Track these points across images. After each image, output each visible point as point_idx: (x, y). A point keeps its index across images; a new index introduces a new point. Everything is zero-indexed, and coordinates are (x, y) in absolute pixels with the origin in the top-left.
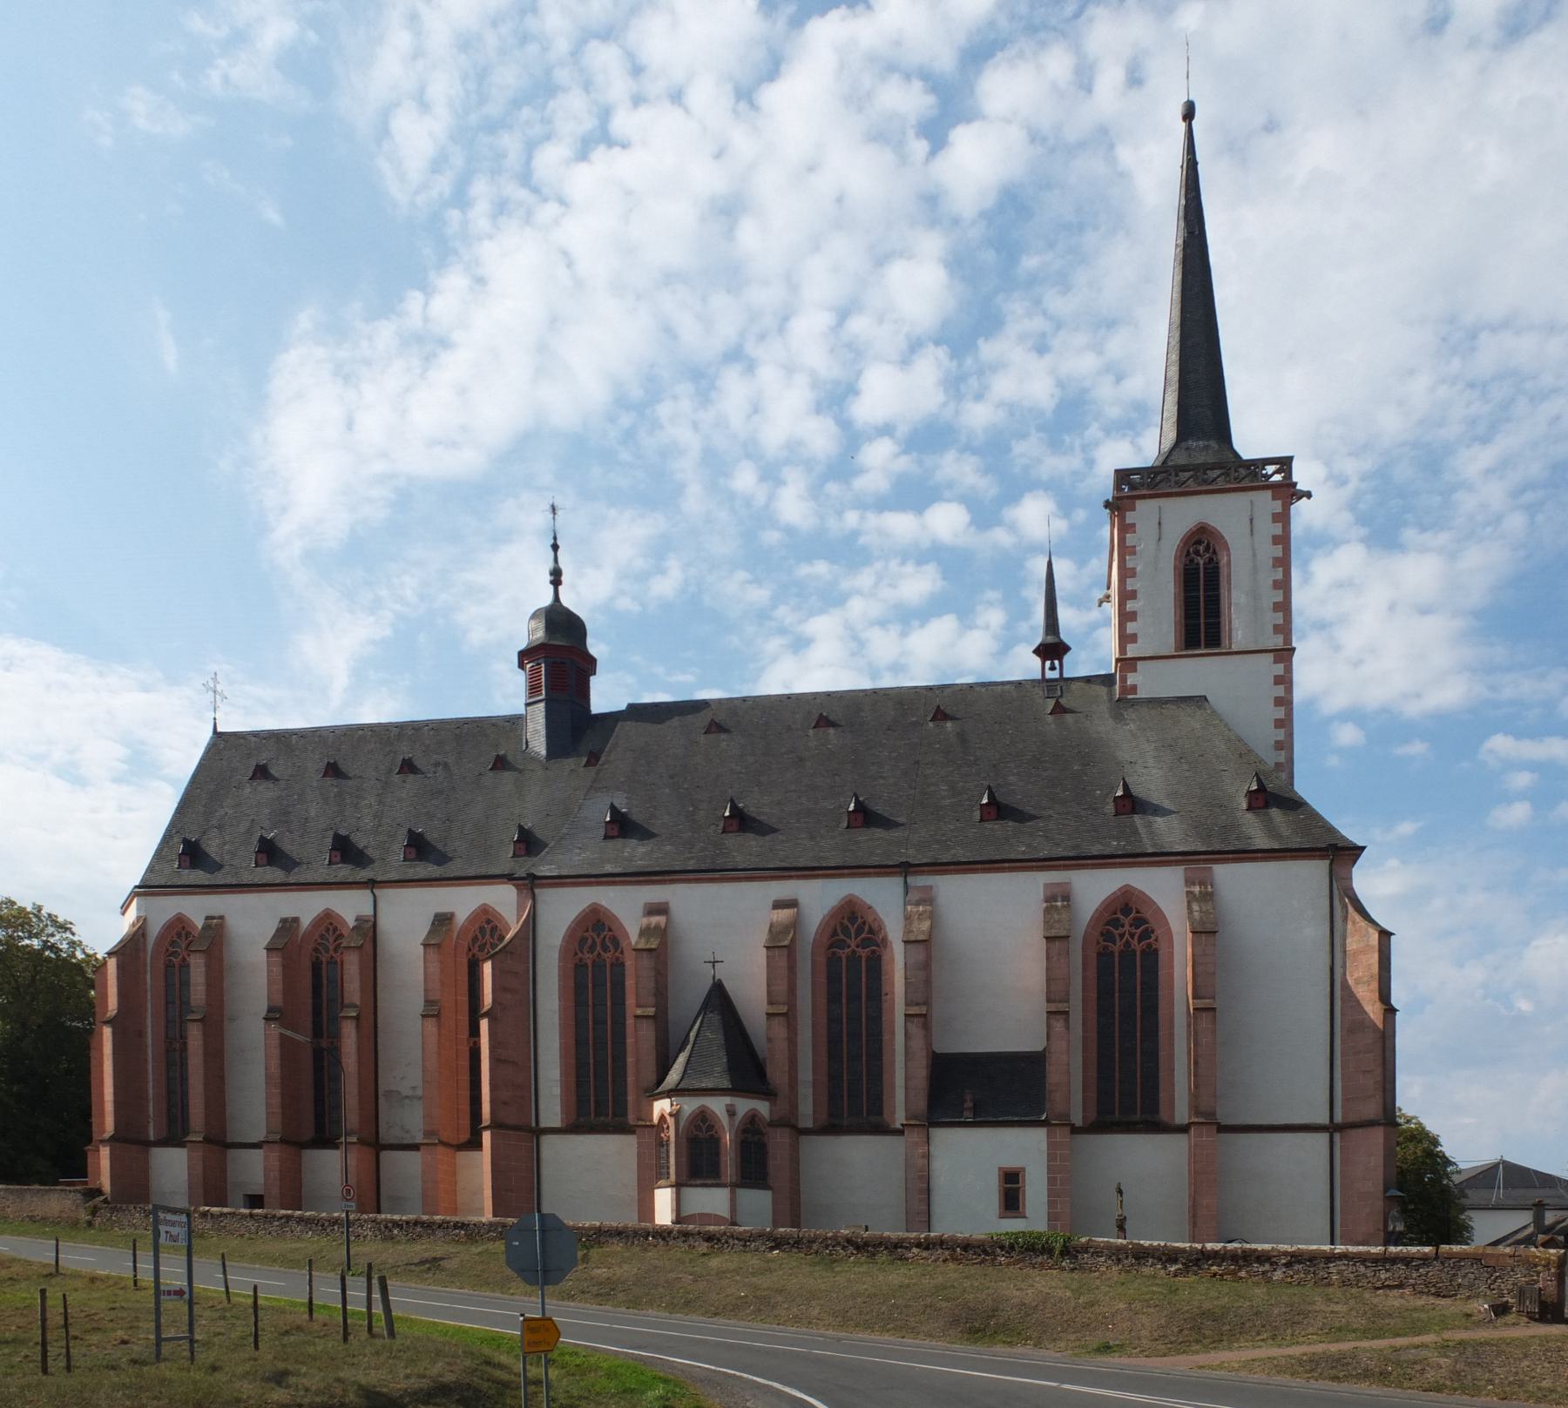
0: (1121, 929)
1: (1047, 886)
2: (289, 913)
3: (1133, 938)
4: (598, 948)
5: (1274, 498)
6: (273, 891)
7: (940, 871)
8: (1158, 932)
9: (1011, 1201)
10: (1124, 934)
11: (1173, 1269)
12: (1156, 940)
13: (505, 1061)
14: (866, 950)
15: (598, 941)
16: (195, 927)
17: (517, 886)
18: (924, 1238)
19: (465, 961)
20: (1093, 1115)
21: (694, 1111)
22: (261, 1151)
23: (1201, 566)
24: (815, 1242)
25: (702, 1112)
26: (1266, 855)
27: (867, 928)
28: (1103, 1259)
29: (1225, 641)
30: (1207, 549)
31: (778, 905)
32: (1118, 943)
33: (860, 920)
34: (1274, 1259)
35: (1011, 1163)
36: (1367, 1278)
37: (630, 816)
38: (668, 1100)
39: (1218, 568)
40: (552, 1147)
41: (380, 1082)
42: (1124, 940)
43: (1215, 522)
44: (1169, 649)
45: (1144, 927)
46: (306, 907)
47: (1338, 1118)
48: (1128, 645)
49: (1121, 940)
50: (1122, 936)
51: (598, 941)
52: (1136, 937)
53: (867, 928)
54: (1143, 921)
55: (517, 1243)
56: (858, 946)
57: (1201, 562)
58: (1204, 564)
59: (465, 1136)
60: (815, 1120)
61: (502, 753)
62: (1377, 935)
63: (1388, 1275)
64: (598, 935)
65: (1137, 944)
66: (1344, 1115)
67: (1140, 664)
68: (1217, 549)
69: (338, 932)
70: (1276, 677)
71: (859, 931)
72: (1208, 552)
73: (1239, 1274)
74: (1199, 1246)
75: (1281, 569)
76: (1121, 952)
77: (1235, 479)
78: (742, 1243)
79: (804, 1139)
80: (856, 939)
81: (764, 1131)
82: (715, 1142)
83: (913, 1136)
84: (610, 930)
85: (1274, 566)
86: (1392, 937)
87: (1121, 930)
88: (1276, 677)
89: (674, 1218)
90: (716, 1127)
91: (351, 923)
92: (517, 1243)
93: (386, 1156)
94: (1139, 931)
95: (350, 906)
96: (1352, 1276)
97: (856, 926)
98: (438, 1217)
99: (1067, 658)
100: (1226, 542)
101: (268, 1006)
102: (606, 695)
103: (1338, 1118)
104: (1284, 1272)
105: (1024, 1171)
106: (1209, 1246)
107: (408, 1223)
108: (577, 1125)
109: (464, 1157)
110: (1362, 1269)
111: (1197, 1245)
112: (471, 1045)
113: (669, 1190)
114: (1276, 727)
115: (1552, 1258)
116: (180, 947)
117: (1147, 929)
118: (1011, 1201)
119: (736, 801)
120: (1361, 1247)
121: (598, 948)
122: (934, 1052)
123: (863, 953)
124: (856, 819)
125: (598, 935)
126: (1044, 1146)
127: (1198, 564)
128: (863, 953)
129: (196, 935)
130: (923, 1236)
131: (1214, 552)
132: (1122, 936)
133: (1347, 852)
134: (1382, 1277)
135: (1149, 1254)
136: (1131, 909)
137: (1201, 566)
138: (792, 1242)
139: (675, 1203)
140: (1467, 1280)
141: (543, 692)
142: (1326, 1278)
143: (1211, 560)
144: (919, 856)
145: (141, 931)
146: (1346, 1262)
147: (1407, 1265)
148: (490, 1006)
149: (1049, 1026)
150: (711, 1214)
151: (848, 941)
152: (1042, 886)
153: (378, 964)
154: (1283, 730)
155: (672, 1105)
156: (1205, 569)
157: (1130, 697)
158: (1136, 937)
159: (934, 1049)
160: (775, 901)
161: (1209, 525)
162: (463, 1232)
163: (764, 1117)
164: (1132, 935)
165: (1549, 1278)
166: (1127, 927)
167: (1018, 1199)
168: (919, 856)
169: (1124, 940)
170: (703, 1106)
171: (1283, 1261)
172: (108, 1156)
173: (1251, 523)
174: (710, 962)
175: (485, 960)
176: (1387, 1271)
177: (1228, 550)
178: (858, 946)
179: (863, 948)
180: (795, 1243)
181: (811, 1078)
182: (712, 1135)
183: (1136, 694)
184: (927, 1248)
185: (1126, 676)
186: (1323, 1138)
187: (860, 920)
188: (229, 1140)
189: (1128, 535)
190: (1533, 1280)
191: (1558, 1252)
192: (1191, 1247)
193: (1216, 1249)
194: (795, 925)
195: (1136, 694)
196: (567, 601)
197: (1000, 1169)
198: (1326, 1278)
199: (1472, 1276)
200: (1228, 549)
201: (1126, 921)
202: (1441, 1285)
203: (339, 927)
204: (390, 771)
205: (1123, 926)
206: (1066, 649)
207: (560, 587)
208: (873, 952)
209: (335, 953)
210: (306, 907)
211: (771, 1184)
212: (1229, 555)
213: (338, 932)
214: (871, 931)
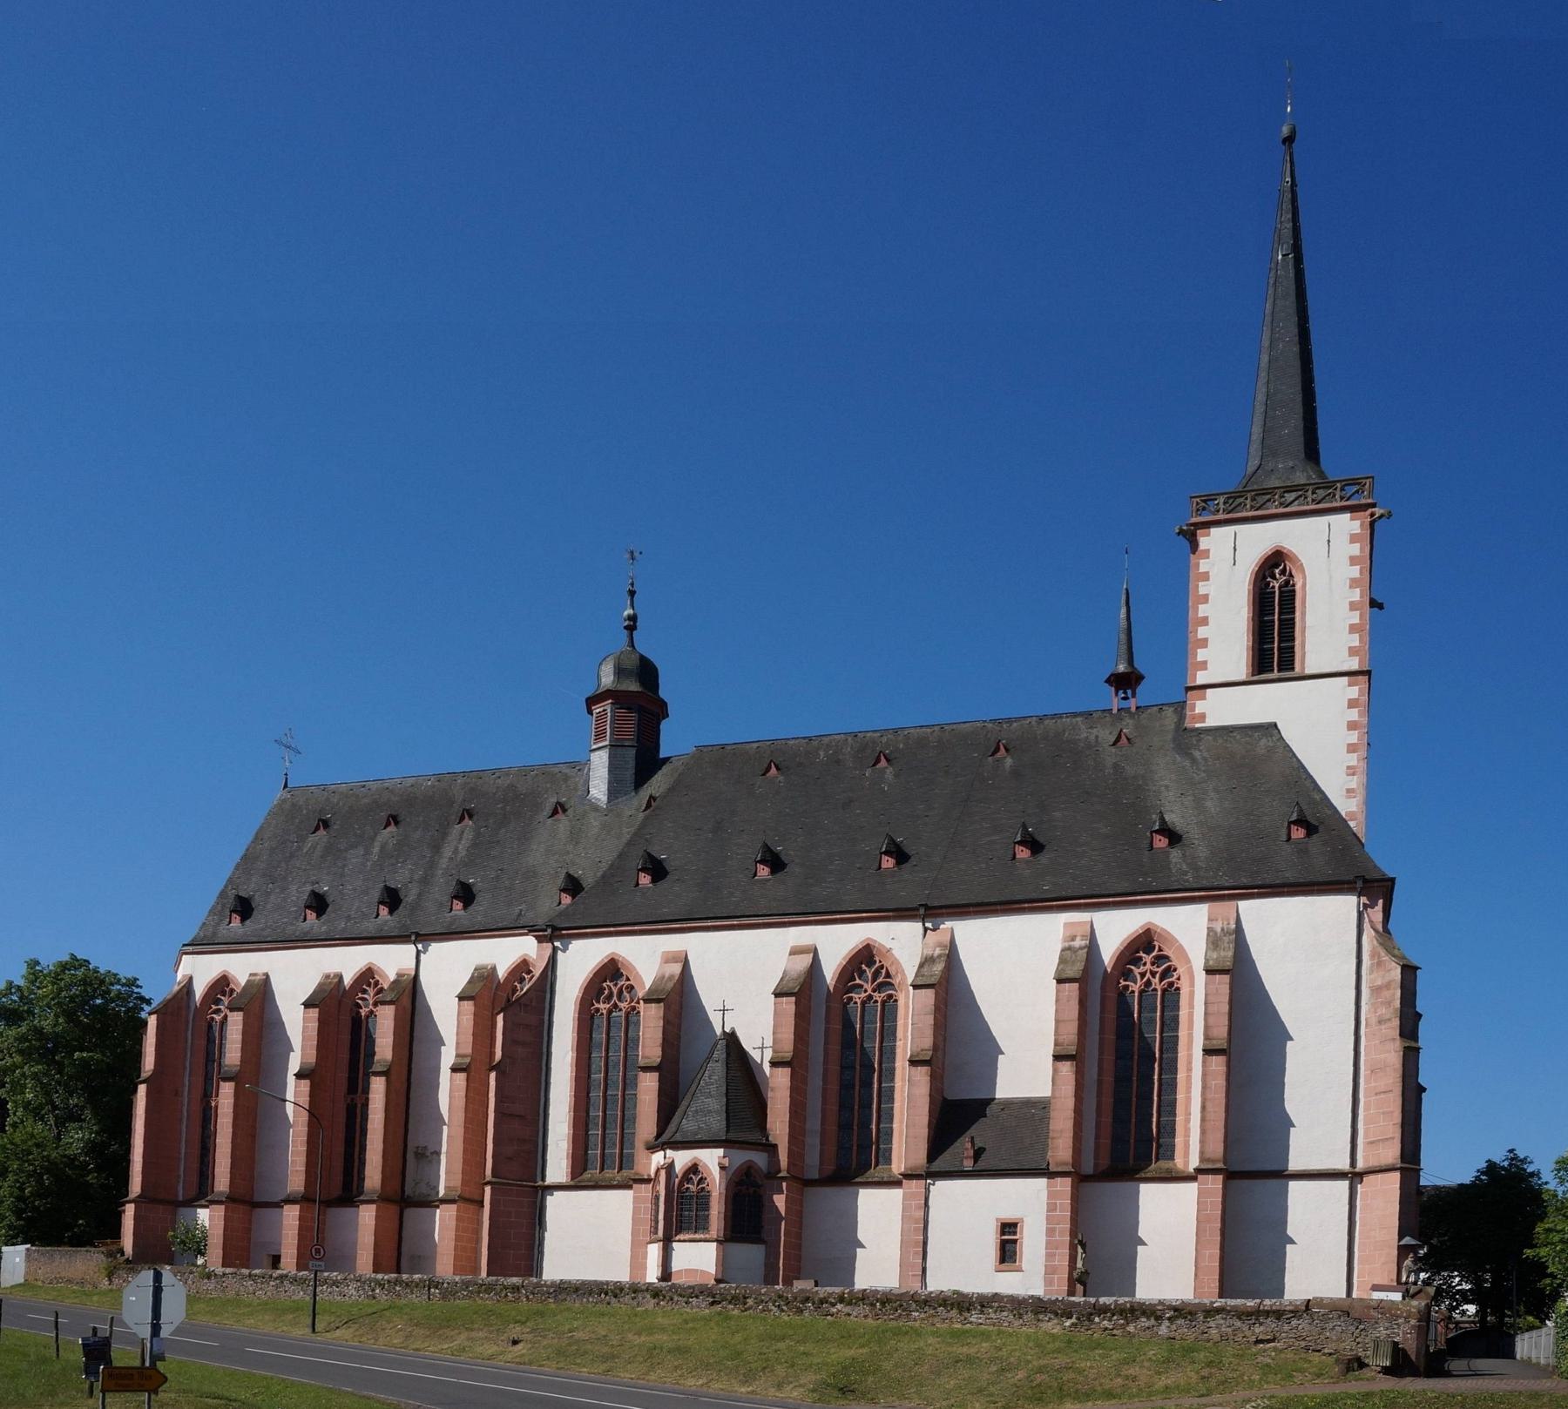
0: (1142, 967)
1: (1066, 925)
2: (333, 969)
3: (1154, 977)
4: (615, 998)
5: (1352, 519)
6: (480, 938)
7: (1304, 891)
8: (1181, 970)
9: (1008, 1252)
10: (1146, 972)
14: (882, 995)
15: (615, 991)
16: (237, 984)
18: (848, 1293)
20: (1105, 1163)
21: (687, 1163)
22: (208, 1210)
24: (750, 1297)
25: (749, 1168)
27: (884, 971)
28: (1005, 1314)
30: (1283, 572)
31: (795, 952)
33: (877, 964)
34: (1159, 1313)
35: (1009, 1215)
36: (1243, 1332)
38: (662, 1153)
39: (1294, 591)
42: (1145, 979)
43: (1290, 545)
45: (1165, 965)
46: (347, 962)
47: (1361, 1165)
48: (1198, 673)
49: (1142, 979)
50: (1143, 975)
51: (615, 991)
52: (1158, 976)
53: (884, 971)
54: (1162, 958)
55: (134, 1299)
56: (874, 991)
57: (1277, 585)
58: (1280, 587)
63: (1262, 1328)
65: (1158, 983)
67: (1209, 691)
68: (1294, 572)
69: (379, 986)
70: (1350, 701)
71: (876, 974)
72: (1285, 576)
73: (1128, 1329)
74: (1092, 1300)
75: (1358, 590)
76: (1141, 992)
77: (1313, 500)
78: (685, 1299)
79: (811, 1192)
80: (872, 984)
82: (703, 1199)
83: (915, 1186)
84: (628, 979)
85: (1351, 587)
86: (1418, 972)
87: (1142, 969)
88: (1350, 701)
89: (660, 1275)
90: (708, 1180)
92: (134, 1299)
93: (410, 1213)
94: (1160, 970)
95: (392, 960)
97: (873, 970)
98: (417, 1276)
100: (1302, 564)
101: (301, 1063)
102: (674, 739)
104: (1169, 1327)
105: (1023, 1221)
106: (1102, 1300)
107: (389, 1281)
108: (580, 1180)
109: (345, 1212)
111: (1091, 1299)
112: (349, 1101)
114: (1349, 752)
115: (1413, 1310)
116: (223, 1005)
117: (1170, 967)
118: (1008, 1252)
120: (1239, 1300)
121: (615, 998)
122: (945, 1099)
123: (878, 997)
124: (1160, 840)
125: (616, 985)
126: (1044, 1195)
128: (878, 997)
131: (1291, 575)
133: (1376, 884)
134: (1257, 1331)
135: (1047, 1308)
138: (730, 1298)
141: (608, 737)
142: (1206, 1333)
143: (1287, 583)
144: (1231, 881)
145: (185, 990)
146: (1225, 1316)
147: (1278, 1319)
148: (150, 1073)
149: (1055, 1071)
150: (697, 1270)
152: (1062, 925)
154: (1356, 754)
155: (665, 1157)
157: (1197, 725)
158: (1158, 976)
159: (946, 1096)
161: (1285, 548)
162: (437, 1291)
163: (761, 1170)
164: (1153, 974)
165: (1409, 1331)
166: (1148, 966)
168: (1231, 881)
169: (1145, 979)
171: (1167, 1315)
172: (133, 1217)
173: (1329, 544)
174: (720, 1010)
175: (498, 1013)
178: (874, 991)
179: (879, 993)
180: (733, 1299)
182: (704, 1188)
183: (1204, 722)
184: (850, 1304)
185: (1195, 704)
186: (1344, 1185)
187: (877, 964)
188: (257, 1199)
189: (1201, 561)
190: (1394, 1333)
191: (1420, 1303)
192: (1085, 1301)
195: (1204, 722)
196: (643, 648)
197: (997, 1219)
198: (1206, 1333)
199: (1339, 1329)
200: (1303, 571)
201: (1147, 958)
202: (1311, 1338)
203: (381, 981)
204: (637, 810)
205: (1145, 964)
207: (635, 632)
208: (890, 996)
209: (375, 1008)
210: (347, 962)
211: (766, 1239)
212: (1304, 578)
213: (379, 986)
214: (888, 975)
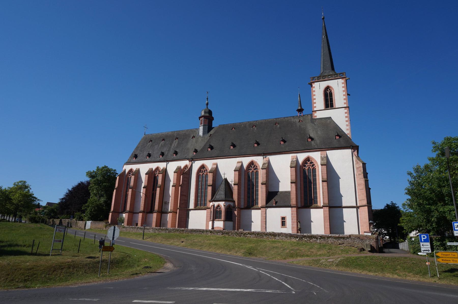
2: (151, 167)
8: (316, 165)
9: (283, 224)
11: (297, 239)
12: (315, 167)
13: (183, 195)
15: (203, 170)
16: (134, 170)
17: (189, 161)
19: (154, 177)
20: (303, 204)
23: (329, 93)
25: (230, 206)
26: (337, 148)
27: (256, 166)
29: (334, 107)
30: (330, 90)
31: (238, 162)
32: (307, 168)
35: (283, 216)
37: (213, 147)
39: (332, 93)
40: (191, 213)
41: (164, 199)
43: (330, 85)
44: (323, 109)
46: (154, 166)
47: (358, 205)
50: (308, 166)
52: (311, 166)
53: (256, 166)
57: (328, 92)
59: (149, 210)
60: (301, 205)
61: (195, 135)
62: (362, 164)
63: (340, 241)
64: (204, 169)
66: (359, 204)
67: (317, 112)
68: (332, 90)
74: (302, 234)
79: (242, 211)
81: (232, 209)
83: (263, 209)
84: (206, 168)
87: (308, 165)
91: (162, 169)
95: (162, 165)
96: (333, 241)
99: (303, 112)
102: (215, 124)
103: (358, 205)
108: (196, 208)
110: (335, 240)
113: (223, 222)
117: (313, 164)
118: (283, 224)
119: (234, 143)
121: (203, 172)
122: (269, 191)
123: (255, 171)
125: (204, 169)
127: (328, 92)
128: (255, 171)
129: (161, 170)
130: (250, 232)
132: (308, 166)
134: (339, 242)
136: (310, 160)
137: (329, 93)
139: (328, 224)
140: (357, 242)
143: (330, 92)
151: (252, 169)
153: (166, 177)
156: (329, 93)
157: (315, 118)
158: (311, 166)
160: (238, 162)
163: (232, 206)
164: (310, 166)
166: (309, 164)
167: (285, 223)
170: (219, 204)
176: (340, 240)
177: (333, 89)
181: (243, 197)
184: (251, 234)
188: (134, 212)
193: (306, 235)
194: (242, 165)
201: (309, 163)
206: (303, 110)
208: (257, 171)
210: (154, 166)
212: (334, 90)
